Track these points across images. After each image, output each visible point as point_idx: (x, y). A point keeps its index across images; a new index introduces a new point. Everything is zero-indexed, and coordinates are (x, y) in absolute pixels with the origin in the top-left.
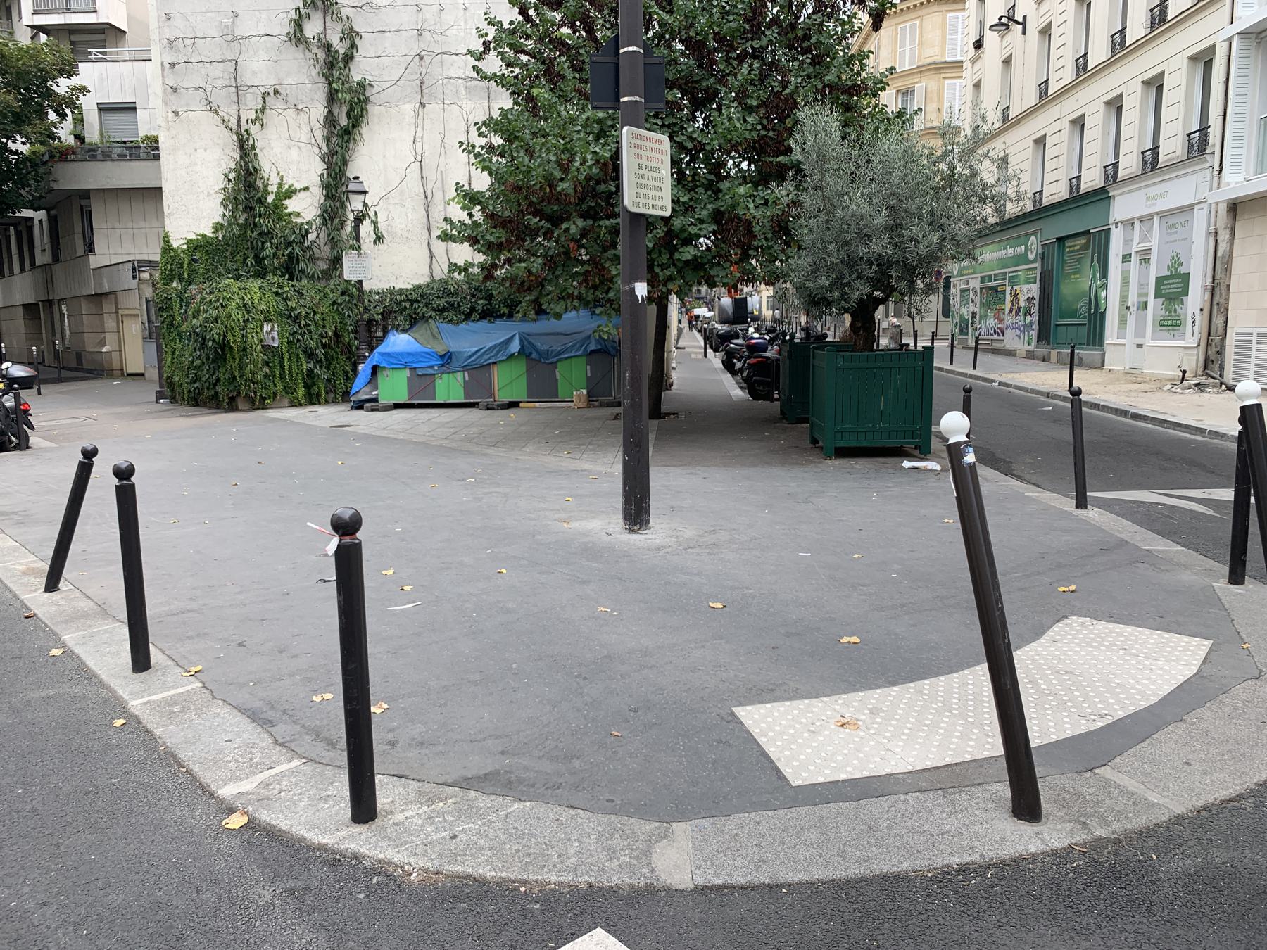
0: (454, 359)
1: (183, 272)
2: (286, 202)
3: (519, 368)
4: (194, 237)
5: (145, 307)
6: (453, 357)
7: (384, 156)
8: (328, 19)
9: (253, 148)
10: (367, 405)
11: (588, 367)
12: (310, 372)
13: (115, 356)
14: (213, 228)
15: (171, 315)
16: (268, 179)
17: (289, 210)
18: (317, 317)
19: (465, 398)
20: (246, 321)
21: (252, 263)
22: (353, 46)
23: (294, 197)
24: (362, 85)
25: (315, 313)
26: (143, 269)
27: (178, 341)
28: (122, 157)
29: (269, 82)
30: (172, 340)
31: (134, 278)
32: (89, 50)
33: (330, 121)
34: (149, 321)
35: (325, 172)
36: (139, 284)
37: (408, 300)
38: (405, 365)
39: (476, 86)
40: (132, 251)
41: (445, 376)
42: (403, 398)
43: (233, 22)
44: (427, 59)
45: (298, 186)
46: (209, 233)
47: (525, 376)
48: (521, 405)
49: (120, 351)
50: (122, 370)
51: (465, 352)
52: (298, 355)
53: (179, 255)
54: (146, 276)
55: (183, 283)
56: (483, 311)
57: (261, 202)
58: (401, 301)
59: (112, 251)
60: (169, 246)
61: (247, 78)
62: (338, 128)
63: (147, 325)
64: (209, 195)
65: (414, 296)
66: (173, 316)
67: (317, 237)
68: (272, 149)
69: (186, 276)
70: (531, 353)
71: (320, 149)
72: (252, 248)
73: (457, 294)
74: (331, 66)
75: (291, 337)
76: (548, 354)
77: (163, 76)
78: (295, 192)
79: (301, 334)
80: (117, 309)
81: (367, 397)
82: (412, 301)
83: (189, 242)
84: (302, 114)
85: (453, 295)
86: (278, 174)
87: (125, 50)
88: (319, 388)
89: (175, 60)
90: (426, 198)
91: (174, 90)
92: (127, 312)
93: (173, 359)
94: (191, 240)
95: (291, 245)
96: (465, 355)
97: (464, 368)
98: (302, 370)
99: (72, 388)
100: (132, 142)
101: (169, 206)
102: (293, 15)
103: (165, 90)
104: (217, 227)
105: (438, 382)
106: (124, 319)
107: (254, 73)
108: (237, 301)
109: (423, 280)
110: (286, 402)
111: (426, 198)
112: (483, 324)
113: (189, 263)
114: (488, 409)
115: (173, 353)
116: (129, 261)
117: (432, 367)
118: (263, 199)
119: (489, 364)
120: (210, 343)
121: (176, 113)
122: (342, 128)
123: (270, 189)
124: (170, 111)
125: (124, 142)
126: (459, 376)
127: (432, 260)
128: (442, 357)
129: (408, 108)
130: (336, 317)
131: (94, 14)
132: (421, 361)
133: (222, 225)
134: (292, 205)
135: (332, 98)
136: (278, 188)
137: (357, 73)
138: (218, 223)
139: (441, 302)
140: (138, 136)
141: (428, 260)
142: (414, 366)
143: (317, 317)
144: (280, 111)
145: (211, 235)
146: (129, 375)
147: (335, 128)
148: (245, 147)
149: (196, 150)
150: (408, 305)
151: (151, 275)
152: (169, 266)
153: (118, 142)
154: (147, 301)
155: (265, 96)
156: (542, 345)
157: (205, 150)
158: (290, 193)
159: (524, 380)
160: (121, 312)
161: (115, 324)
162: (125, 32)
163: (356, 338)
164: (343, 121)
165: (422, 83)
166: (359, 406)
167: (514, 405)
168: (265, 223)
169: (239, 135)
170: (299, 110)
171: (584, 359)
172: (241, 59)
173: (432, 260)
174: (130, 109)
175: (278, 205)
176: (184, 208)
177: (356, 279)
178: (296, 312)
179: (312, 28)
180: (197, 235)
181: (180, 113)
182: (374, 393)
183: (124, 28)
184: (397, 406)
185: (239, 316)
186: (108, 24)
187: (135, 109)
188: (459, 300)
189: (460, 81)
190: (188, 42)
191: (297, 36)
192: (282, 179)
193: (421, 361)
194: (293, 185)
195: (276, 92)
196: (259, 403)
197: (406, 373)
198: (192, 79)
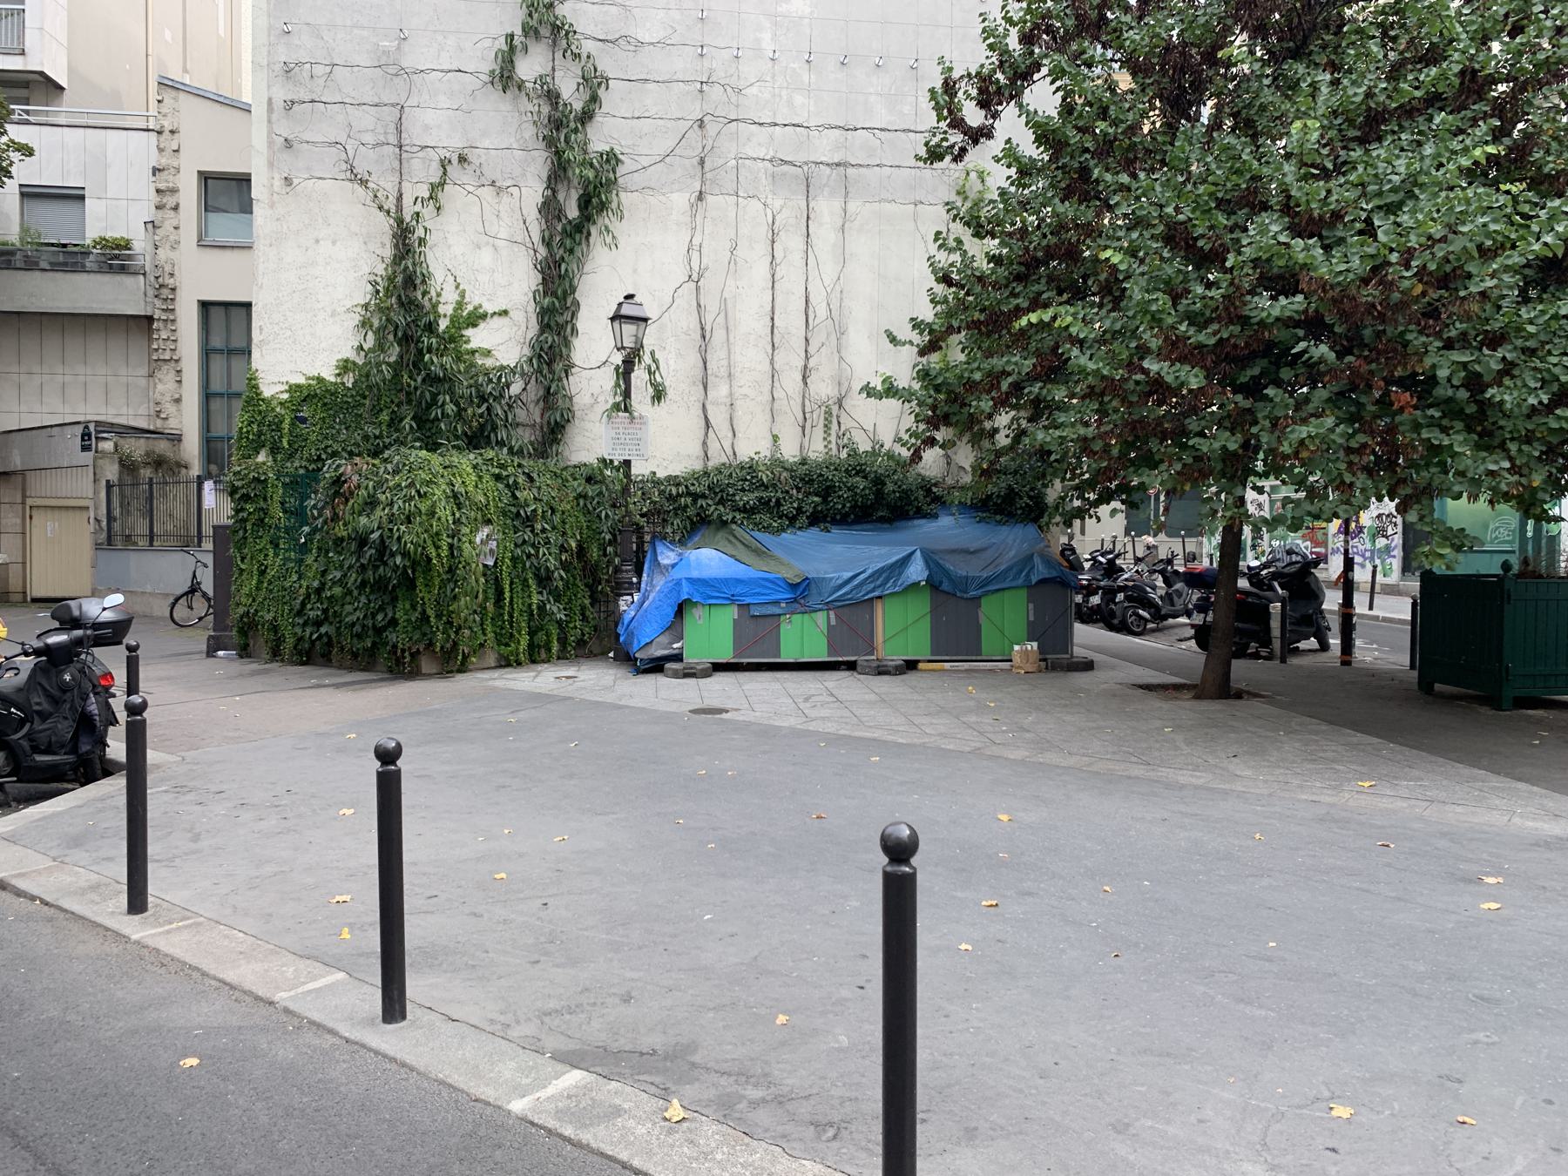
0: (814, 591)
1: (281, 437)
2: (469, 332)
3: (919, 607)
4: (302, 381)
5: (103, 494)
6: (813, 586)
7: (635, 271)
8: (559, 55)
9: (422, 241)
10: (668, 665)
11: (1031, 606)
12: (542, 607)
13: (15, 571)
14: (337, 367)
15: (262, 509)
16: (439, 295)
17: (473, 345)
18: (557, 519)
19: (829, 655)
20: (457, 522)
21: (411, 427)
22: (594, 99)
23: (482, 325)
24: (611, 158)
25: (553, 511)
26: (105, 435)
27: (271, 553)
28: (56, 267)
29: (449, 140)
30: (261, 550)
31: (85, 448)
32: (12, 107)
33: (550, 208)
34: (110, 518)
35: (541, 288)
36: (95, 459)
37: (689, 494)
38: (732, 600)
39: (784, 174)
40: (124, 411)
41: (797, 618)
42: (726, 656)
43: (398, 48)
44: (712, 128)
45: (489, 307)
46: (329, 375)
47: (928, 618)
48: (921, 665)
49: (24, 563)
50: (25, 593)
51: (831, 579)
52: (526, 580)
53: (273, 410)
54: (108, 446)
55: (279, 457)
56: (815, 512)
57: (431, 328)
58: (678, 495)
59: (23, 408)
60: (258, 394)
61: (415, 135)
62: (564, 221)
63: (104, 524)
64: (333, 314)
65: (698, 489)
66: (265, 511)
67: (524, 389)
68: (449, 247)
69: (285, 444)
70: (941, 583)
71: (535, 251)
72: (409, 402)
73: (774, 486)
74: (557, 124)
75: (519, 551)
76: (965, 582)
77: (269, 121)
78: (484, 316)
79: (533, 545)
80: (24, 497)
81: (666, 652)
82: (696, 497)
83: (293, 389)
84: (505, 199)
85: (767, 487)
86: (457, 287)
87: (63, 110)
88: (548, 635)
89: (296, 98)
90: (704, 337)
91: (288, 144)
92: (39, 502)
93: (260, 582)
94: (298, 386)
95: (487, 401)
96: (833, 584)
97: (828, 606)
98: (530, 605)
99: (1355, 740)
100: (75, 245)
101: (261, 329)
102: (502, 44)
103: (271, 143)
104: (345, 366)
105: (785, 628)
106: (35, 513)
107: (427, 128)
108: (443, 487)
109: (698, 466)
110: (491, 659)
111: (704, 337)
112: (814, 532)
113: (292, 424)
114: (880, 674)
115: (262, 573)
116: (78, 423)
117: (776, 603)
118: (434, 325)
119: (872, 599)
120: (398, 560)
121: (288, 181)
122: (570, 222)
123: (441, 309)
124: (277, 176)
125: (64, 246)
126: (821, 617)
127: (706, 434)
128: (794, 587)
129: (681, 200)
130: (582, 519)
131: (21, 57)
132: (758, 594)
133: (354, 363)
134: (477, 338)
135: (558, 173)
136: (455, 310)
137: (600, 138)
138: (346, 361)
139: (750, 498)
140: (84, 239)
141: (703, 432)
142: (748, 600)
143: (557, 519)
144: (471, 189)
145: (333, 379)
146: (35, 600)
147: (560, 220)
148: (405, 243)
149: (317, 241)
150: (689, 500)
151: (116, 445)
152: (255, 426)
153: (53, 245)
154: (109, 486)
155: (444, 164)
156: (960, 568)
157: (334, 243)
158: (476, 318)
159: (925, 626)
160: (29, 502)
161: (19, 521)
162: (62, 89)
163: (616, 554)
164: (573, 212)
165: (702, 162)
166: (656, 666)
167: (911, 665)
168: (435, 363)
169: (400, 221)
170: (500, 191)
171: (1023, 593)
172: (413, 101)
173: (706, 434)
174: (76, 197)
175: (453, 339)
176: (289, 333)
177: (622, 458)
178: (529, 510)
179: (529, 67)
180: (309, 378)
181: (296, 181)
182: (675, 646)
183: (65, 85)
184: (718, 667)
185: (445, 512)
186: (42, 74)
187: (82, 198)
188: (779, 494)
189: (760, 164)
190: (319, 70)
191: (505, 77)
192: (463, 294)
193: (758, 594)
194: (480, 306)
195: (462, 159)
196: (453, 662)
197: (732, 613)
198: (327, 128)
